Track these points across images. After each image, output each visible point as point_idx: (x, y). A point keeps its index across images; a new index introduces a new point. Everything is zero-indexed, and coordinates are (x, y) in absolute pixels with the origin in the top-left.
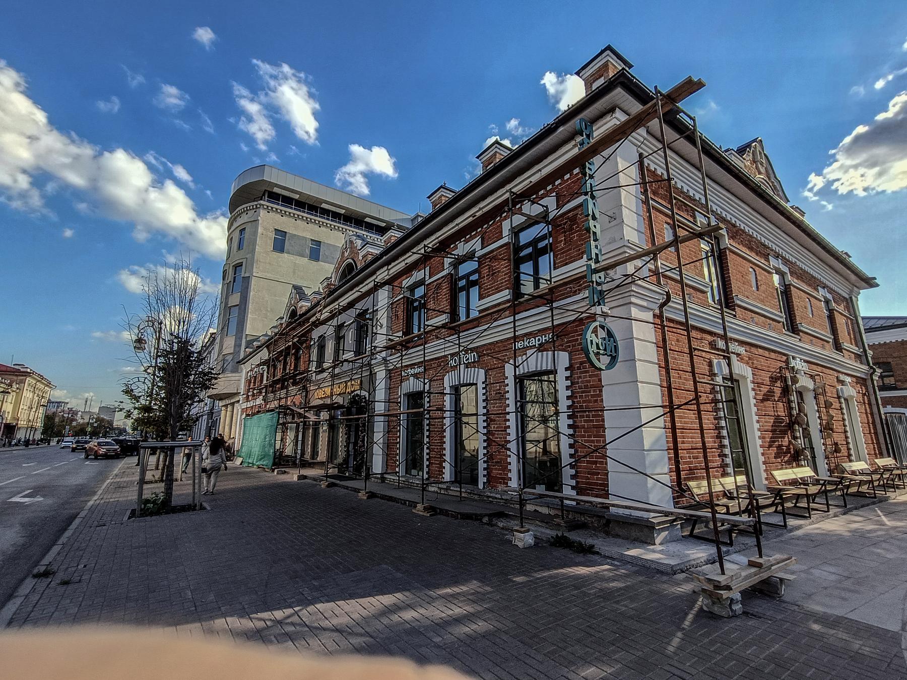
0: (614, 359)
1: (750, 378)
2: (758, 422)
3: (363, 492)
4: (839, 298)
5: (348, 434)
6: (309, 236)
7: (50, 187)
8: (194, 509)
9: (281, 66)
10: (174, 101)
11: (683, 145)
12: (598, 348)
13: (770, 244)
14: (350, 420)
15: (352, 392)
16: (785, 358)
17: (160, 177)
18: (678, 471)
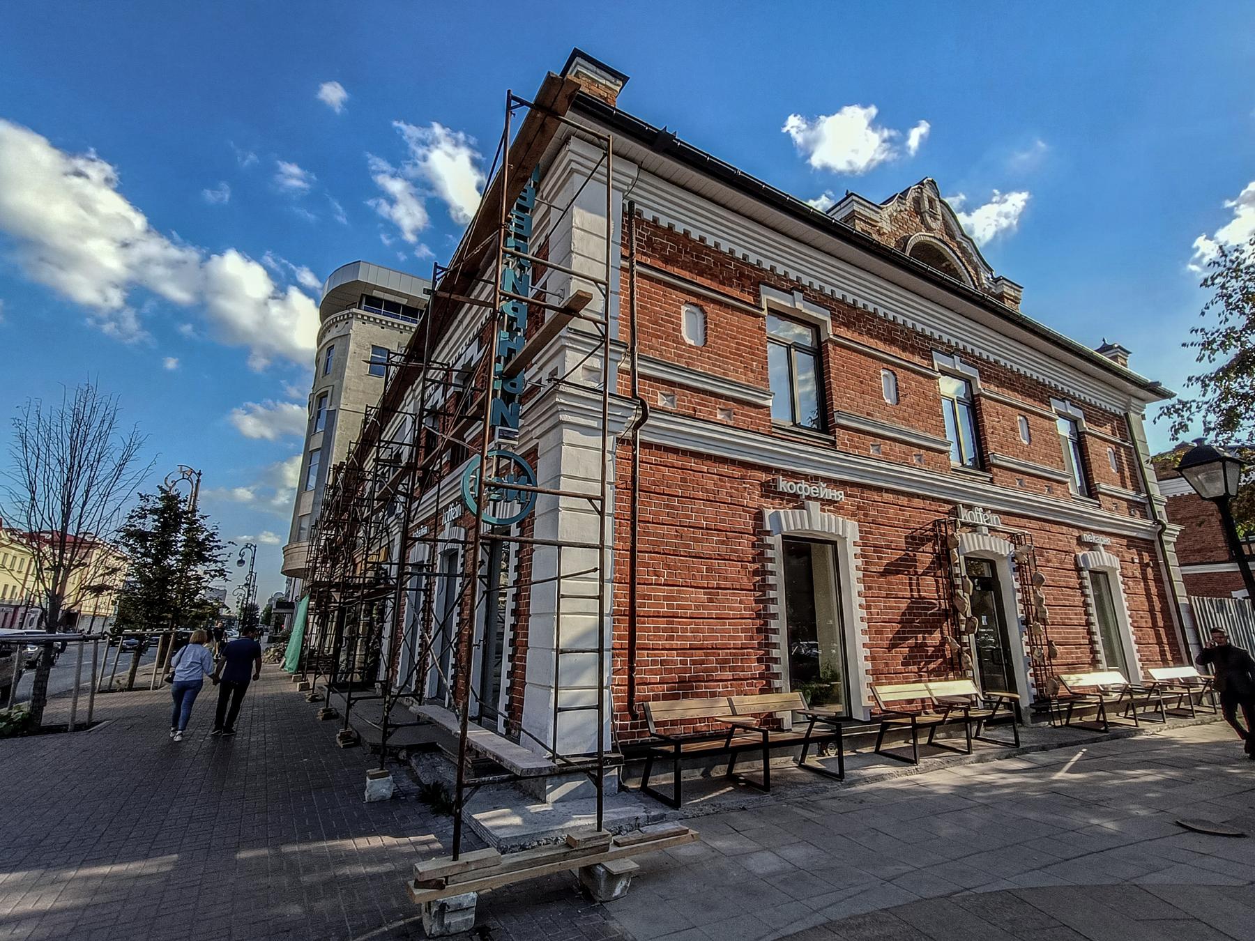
4: (1097, 415)
7: (148, 307)
8: (66, 731)
9: (430, 127)
10: (296, 183)
16: (948, 507)
17: (282, 283)
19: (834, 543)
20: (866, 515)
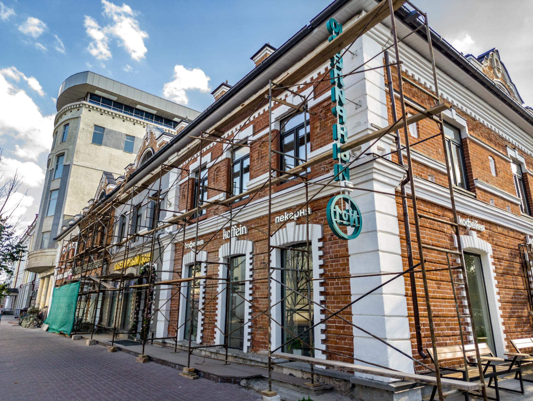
0: (357, 229)
1: (490, 253)
2: (499, 293)
3: (141, 356)
5: (138, 302)
6: (124, 131)
11: (415, 38)
12: (341, 218)
13: (507, 137)
14: (141, 288)
15: (145, 263)
16: (522, 237)
18: (419, 337)
19: (479, 256)
20: (493, 240)
